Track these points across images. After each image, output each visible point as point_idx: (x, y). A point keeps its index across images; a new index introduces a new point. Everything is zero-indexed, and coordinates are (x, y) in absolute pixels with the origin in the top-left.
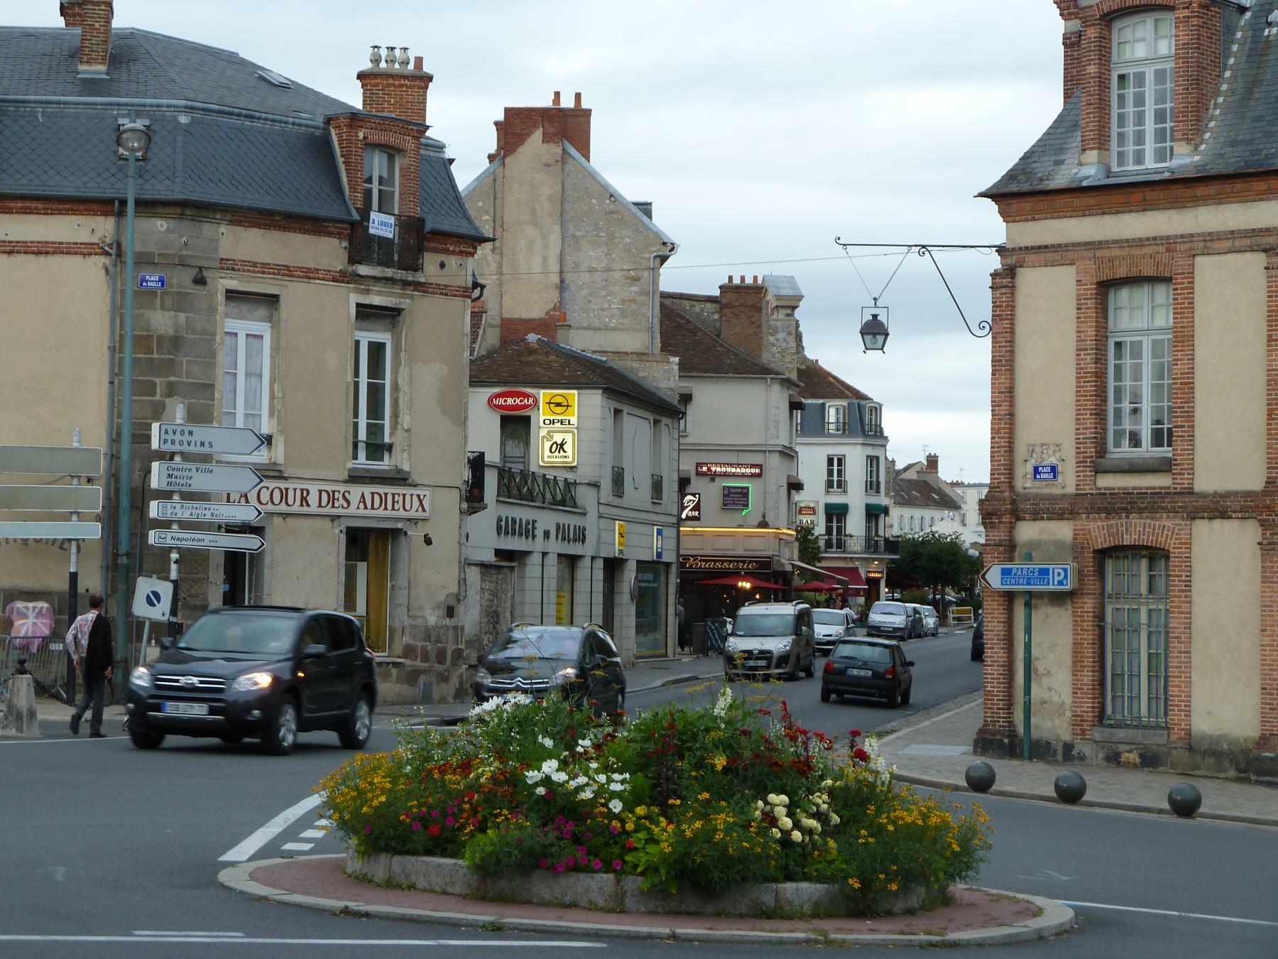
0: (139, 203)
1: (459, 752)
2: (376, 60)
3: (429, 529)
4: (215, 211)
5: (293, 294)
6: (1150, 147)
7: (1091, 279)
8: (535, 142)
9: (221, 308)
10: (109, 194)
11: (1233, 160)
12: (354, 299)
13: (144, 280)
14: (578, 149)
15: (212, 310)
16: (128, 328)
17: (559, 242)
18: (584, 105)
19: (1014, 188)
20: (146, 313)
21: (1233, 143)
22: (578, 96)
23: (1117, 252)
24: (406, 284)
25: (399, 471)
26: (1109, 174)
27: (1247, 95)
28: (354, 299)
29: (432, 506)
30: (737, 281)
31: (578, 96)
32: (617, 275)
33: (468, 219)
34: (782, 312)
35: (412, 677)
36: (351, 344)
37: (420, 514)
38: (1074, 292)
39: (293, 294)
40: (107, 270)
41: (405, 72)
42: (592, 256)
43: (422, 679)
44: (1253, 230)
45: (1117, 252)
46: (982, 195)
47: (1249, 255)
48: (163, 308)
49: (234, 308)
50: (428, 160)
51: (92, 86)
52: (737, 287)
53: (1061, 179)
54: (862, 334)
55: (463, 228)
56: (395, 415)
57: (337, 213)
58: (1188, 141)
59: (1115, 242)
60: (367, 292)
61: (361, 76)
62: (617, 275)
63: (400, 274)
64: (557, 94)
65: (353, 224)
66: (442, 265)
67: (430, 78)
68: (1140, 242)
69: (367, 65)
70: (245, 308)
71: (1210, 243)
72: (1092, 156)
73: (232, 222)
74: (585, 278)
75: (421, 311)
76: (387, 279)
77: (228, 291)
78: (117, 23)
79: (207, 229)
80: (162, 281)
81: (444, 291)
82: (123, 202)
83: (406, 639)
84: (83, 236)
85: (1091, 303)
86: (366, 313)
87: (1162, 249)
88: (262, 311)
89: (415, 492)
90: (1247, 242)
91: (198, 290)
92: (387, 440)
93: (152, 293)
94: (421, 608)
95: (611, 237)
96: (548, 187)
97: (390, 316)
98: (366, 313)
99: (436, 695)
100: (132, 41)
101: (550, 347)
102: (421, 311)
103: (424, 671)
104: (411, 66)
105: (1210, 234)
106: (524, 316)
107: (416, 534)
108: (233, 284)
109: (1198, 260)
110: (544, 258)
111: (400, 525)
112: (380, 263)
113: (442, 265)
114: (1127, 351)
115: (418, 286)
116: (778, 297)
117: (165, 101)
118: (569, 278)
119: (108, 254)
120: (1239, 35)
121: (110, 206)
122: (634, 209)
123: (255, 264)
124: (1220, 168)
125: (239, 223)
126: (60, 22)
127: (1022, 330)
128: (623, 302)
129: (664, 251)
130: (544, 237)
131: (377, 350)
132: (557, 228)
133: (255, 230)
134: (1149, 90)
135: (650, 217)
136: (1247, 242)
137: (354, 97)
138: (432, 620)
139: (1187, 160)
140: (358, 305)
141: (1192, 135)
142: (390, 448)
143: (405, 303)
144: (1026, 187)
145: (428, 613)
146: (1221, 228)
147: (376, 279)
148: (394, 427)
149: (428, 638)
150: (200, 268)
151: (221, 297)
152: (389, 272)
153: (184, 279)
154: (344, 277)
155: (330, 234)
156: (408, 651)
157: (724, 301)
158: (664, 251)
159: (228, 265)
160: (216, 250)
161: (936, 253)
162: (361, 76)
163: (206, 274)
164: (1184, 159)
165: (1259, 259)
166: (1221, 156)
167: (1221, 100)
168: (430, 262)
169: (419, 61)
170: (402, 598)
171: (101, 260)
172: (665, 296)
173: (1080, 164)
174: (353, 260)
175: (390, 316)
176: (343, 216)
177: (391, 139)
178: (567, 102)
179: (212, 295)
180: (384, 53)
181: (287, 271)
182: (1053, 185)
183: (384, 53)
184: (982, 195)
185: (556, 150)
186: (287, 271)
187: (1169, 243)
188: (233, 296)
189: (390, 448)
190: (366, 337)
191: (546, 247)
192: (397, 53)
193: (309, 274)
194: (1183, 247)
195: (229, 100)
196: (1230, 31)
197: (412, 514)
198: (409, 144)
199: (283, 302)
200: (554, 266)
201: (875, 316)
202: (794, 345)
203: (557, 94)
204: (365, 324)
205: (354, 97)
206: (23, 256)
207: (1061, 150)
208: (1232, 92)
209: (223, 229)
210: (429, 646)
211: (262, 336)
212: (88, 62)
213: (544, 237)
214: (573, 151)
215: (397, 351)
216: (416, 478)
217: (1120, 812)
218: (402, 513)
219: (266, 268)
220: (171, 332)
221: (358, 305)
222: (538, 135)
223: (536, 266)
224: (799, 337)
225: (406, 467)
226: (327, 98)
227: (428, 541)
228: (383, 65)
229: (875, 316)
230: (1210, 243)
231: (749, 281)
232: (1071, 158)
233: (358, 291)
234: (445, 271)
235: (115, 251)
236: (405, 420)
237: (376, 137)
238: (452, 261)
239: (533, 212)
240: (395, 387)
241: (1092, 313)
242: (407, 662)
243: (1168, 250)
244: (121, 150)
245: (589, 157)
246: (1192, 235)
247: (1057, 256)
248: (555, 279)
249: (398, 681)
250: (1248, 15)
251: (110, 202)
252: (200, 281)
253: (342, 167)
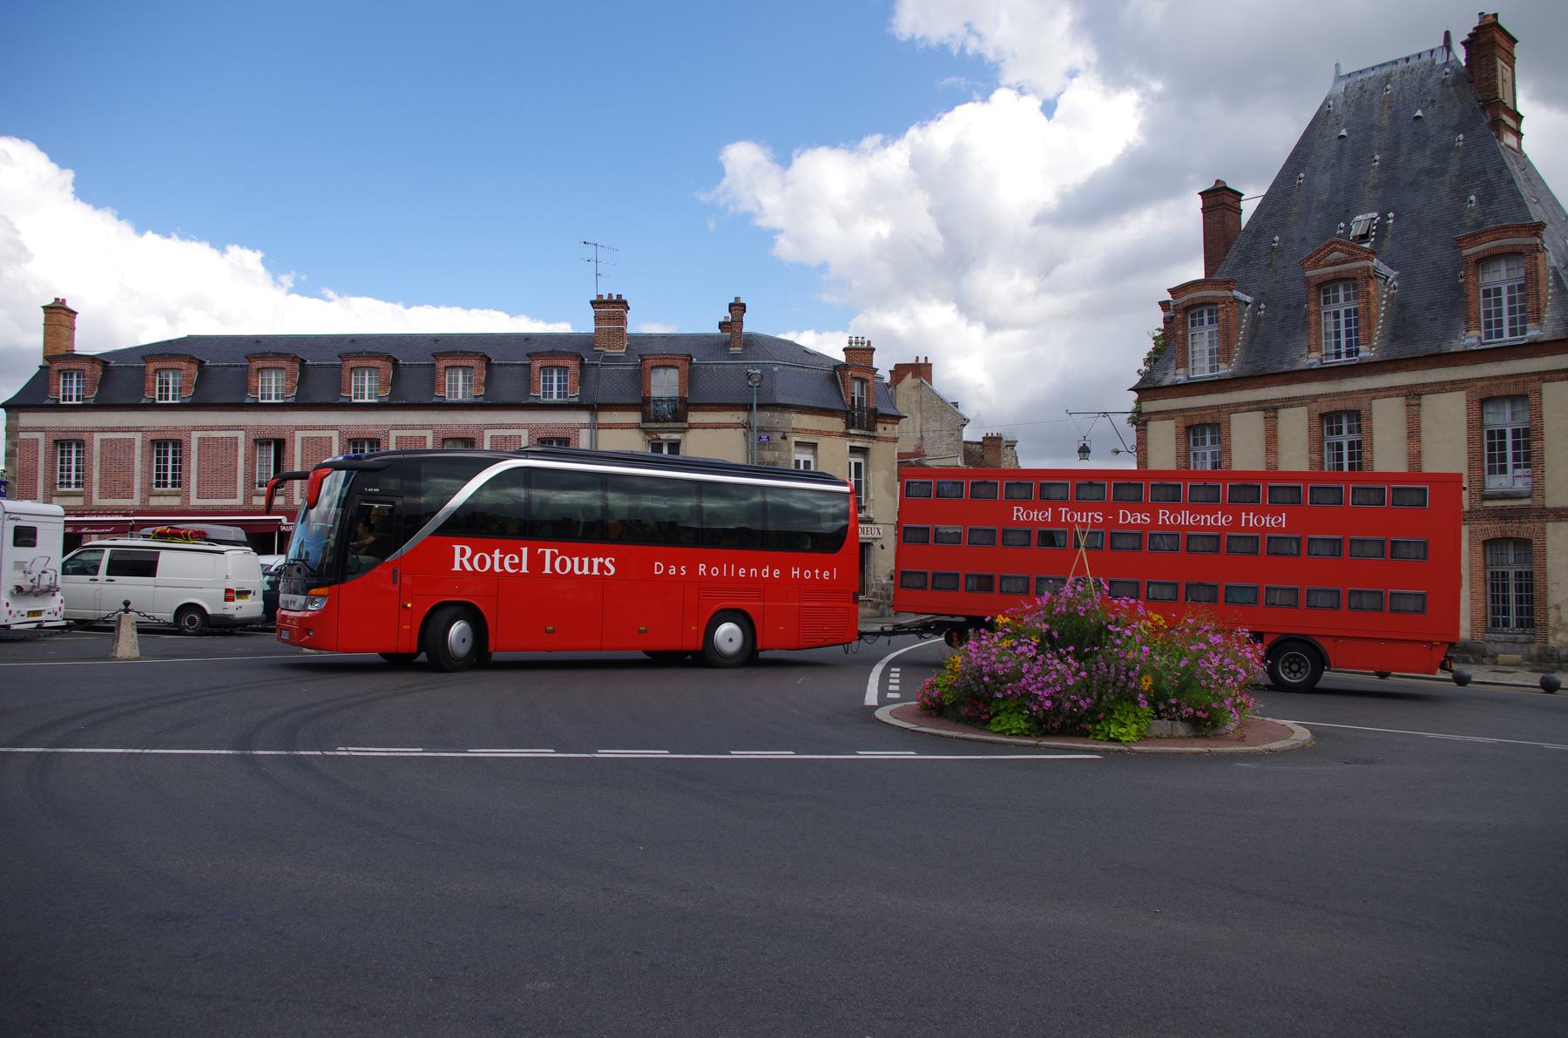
0: (757, 405)
1: (989, 649)
2: (850, 343)
3: (881, 542)
4: (791, 408)
5: (823, 443)
6: (1506, 328)
7: (1182, 425)
8: (909, 380)
9: (793, 449)
10: (746, 402)
11: (1246, 371)
12: (849, 444)
13: (760, 438)
14: (927, 381)
15: (790, 450)
16: (755, 458)
17: (920, 420)
18: (929, 362)
19: (1145, 386)
20: (763, 452)
21: (1246, 363)
22: (926, 358)
23: (1195, 413)
24: (870, 437)
25: (870, 518)
26: (1189, 378)
27: (1251, 342)
28: (849, 444)
29: (883, 533)
30: (990, 435)
31: (926, 358)
32: (945, 433)
33: (896, 410)
34: (1009, 448)
35: (876, 606)
36: (848, 463)
37: (878, 536)
38: (1174, 431)
39: (823, 443)
40: (745, 434)
41: (862, 347)
42: (934, 425)
43: (881, 607)
44: (1258, 401)
45: (1195, 413)
46: (1130, 390)
47: (1256, 412)
48: (769, 450)
49: (798, 450)
50: (877, 383)
51: (735, 356)
52: (990, 438)
53: (1167, 381)
54: (1079, 452)
55: (893, 412)
56: (867, 494)
57: (841, 407)
58: (1226, 362)
59: (1193, 408)
60: (854, 441)
61: (845, 350)
62: (945, 433)
63: (867, 433)
64: (917, 357)
65: (847, 412)
66: (885, 429)
67: (874, 349)
68: (1205, 408)
69: (847, 345)
70: (803, 450)
71: (1237, 408)
72: (1181, 371)
73: (797, 412)
74: (932, 434)
75: (877, 449)
76: (863, 435)
77: (796, 442)
78: (744, 330)
79: (787, 416)
80: (768, 438)
81: (886, 440)
82: (752, 405)
83: (874, 590)
84: (735, 420)
85: (1182, 436)
86: (853, 450)
87: (1215, 411)
88: (810, 451)
89: (876, 526)
90: (1255, 406)
91: (783, 441)
92: (863, 504)
93: (764, 443)
94: (879, 577)
95: (942, 417)
96: (914, 396)
97: (864, 451)
98: (853, 450)
99: (887, 613)
100: (751, 338)
101: (919, 464)
102: (877, 449)
103: (882, 604)
104: (866, 345)
105: (1238, 403)
106: (906, 451)
107: (877, 544)
108: (798, 439)
109: (1232, 415)
110: (914, 427)
111: (870, 541)
112: (859, 428)
113: (885, 429)
114: (1200, 457)
115: (874, 438)
116: (1007, 442)
117: (767, 362)
118: (925, 434)
119: (745, 427)
120: (1246, 315)
121: (747, 407)
122: (952, 405)
123: (807, 430)
124: (1241, 374)
125: (800, 413)
126: (719, 331)
127: (1150, 448)
128: (948, 445)
129: (965, 421)
130: (914, 418)
131: (858, 465)
132: (919, 415)
133: (806, 416)
134: (1505, 297)
135: (957, 407)
136: (1255, 406)
137: (842, 357)
138: (884, 582)
139: (1226, 371)
140: (850, 447)
141: (1227, 360)
142: (865, 508)
143: (870, 445)
144: (1151, 385)
145: (882, 578)
146: (1253, 400)
147: (858, 435)
148: (866, 498)
149: (883, 589)
150: (784, 433)
151: (793, 445)
152: (863, 432)
153: (777, 437)
154: (847, 435)
155: (838, 417)
156: (875, 595)
157: (985, 443)
158: (965, 421)
159: (796, 431)
160: (790, 425)
161: (1113, 417)
162: (845, 350)
163: (787, 434)
164: (1224, 370)
165: (1261, 414)
166: (1241, 368)
167: (1239, 344)
168: (880, 427)
169: (869, 342)
170: (872, 572)
171: (742, 430)
172: (966, 442)
173: (1176, 374)
174: (847, 428)
175: (864, 451)
176: (844, 409)
177: (862, 375)
178: (922, 361)
179: (790, 443)
180: (854, 339)
181: (820, 433)
182: (1164, 384)
183: (854, 339)
184: (1130, 390)
185: (917, 381)
186: (820, 433)
187: (1218, 408)
188: (798, 444)
189: (865, 508)
190: (853, 460)
191: (914, 422)
192: (860, 339)
193: (829, 434)
194: (1225, 410)
195: (793, 360)
196: (1242, 313)
197: (875, 536)
198: (869, 377)
199: (819, 445)
200: (918, 430)
201: (1084, 445)
202: (1014, 461)
203: (917, 357)
204: (854, 455)
205: (842, 357)
206: (710, 430)
207: (1166, 368)
208: (1244, 340)
209: (793, 415)
210: (883, 592)
211: (796, 461)
212: (734, 346)
213: (914, 418)
214: (924, 381)
215: (867, 466)
216: (876, 520)
217: (1429, 681)
218: (870, 536)
219: (811, 432)
220: (773, 460)
221: (850, 447)
222: (910, 374)
223: (911, 429)
224: (1017, 458)
225: (872, 516)
226: (833, 359)
227: (883, 547)
228: (854, 345)
229: (1084, 445)
230: (1237, 408)
231: (995, 435)
232: (1171, 372)
233: (850, 441)
234: (886, 432)
235: (747, 426)
236: (872, 496)
237: (856, 374)
238: (889, 427)
239: (909, 408)
240: (866, 482)
241: (1183, 440)
242: (874, 600)
243: (1218, 412)
244: (750, 383)
245: (931, 379)
246: (1229, 404)
247: (1166, 416)
248: (918, 435)
249: (871, 607)
250: (1250, 306)
251: (745, 405)
252: (784, 438)
253: (842, 387)
